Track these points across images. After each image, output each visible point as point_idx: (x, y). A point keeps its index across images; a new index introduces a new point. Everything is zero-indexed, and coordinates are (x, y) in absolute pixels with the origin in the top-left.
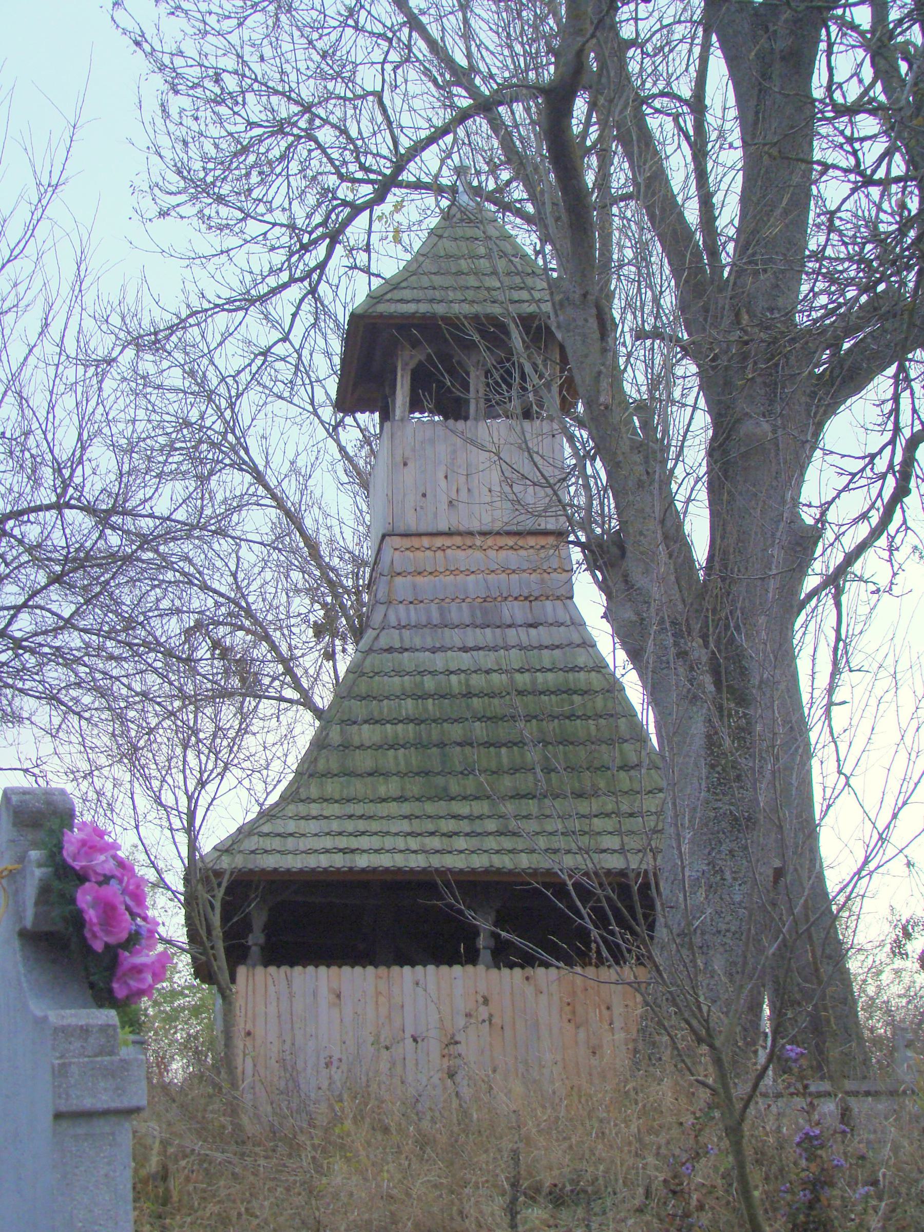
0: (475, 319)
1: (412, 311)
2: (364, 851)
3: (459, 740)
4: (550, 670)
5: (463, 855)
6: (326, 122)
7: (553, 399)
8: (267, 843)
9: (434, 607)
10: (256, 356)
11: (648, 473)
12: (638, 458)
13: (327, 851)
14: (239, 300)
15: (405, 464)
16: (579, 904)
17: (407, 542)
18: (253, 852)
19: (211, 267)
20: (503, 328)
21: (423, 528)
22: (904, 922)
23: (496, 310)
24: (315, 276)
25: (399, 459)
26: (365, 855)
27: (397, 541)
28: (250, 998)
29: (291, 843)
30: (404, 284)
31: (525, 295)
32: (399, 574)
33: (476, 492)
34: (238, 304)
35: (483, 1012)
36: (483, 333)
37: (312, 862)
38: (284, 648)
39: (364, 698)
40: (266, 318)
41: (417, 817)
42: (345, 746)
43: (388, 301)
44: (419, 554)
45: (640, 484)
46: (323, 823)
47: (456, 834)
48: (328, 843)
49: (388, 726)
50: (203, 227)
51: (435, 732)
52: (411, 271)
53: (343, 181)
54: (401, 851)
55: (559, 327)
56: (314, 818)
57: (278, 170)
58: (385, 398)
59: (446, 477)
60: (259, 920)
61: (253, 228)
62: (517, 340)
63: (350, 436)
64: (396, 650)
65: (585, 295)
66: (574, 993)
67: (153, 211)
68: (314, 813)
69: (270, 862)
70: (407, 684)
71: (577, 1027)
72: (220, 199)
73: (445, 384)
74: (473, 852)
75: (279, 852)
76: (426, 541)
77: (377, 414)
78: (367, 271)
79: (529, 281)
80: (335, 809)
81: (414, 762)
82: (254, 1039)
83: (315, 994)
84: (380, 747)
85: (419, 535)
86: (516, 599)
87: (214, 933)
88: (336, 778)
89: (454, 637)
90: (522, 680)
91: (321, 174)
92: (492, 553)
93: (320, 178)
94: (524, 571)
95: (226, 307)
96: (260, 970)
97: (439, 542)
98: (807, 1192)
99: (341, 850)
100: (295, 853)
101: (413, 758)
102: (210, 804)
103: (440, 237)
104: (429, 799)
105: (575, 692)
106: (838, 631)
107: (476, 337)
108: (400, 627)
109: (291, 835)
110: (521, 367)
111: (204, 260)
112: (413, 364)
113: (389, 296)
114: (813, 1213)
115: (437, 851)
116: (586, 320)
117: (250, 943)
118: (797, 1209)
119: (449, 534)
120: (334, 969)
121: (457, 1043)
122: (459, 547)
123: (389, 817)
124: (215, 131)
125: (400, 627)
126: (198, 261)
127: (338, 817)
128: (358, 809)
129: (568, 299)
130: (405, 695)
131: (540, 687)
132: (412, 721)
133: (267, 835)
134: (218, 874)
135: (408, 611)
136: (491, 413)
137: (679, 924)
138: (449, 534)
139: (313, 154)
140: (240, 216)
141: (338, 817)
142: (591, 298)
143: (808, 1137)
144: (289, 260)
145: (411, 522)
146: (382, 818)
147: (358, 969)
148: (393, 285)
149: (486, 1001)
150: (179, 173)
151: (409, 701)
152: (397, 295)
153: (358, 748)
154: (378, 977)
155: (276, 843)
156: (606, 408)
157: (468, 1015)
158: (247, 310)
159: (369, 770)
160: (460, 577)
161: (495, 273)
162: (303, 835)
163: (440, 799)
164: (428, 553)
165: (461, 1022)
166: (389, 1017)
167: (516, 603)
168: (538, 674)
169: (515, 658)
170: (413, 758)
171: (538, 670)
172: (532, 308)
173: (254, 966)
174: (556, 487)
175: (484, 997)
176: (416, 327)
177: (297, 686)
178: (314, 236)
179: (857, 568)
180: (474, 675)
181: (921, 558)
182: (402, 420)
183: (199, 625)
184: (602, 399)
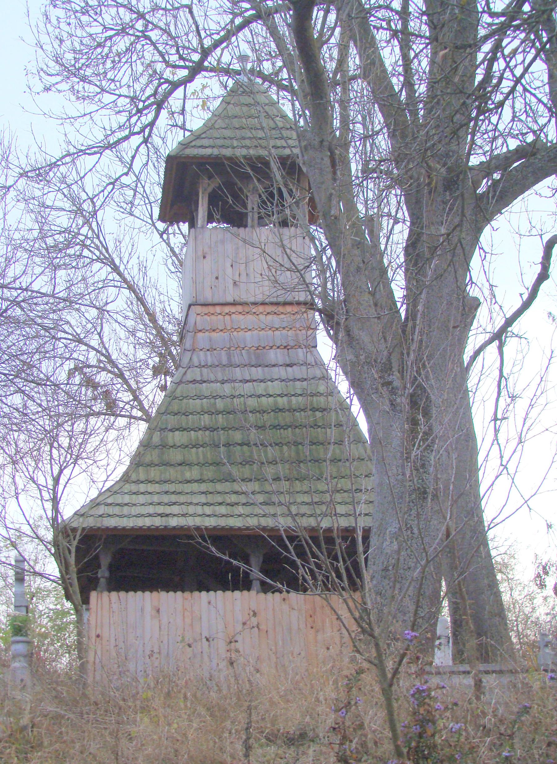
0: (248, 158)
1: (209, 154)
2: (174, 515)
3: (240, 442)
4: (301, 395)
5: (240, 518)
6: (156, 27)
7: (303, 212)
8: (110, 510)
9: (223, 353)
10: (108, 185)
11: (364, 262)
12: (357, 252)
13: (150, 515)
14: (97, 147)
15: (204, 257)
16: (288, 543)
17: (206, 310)
18: (100, 516)
19: (77, 125)
20: (267, 164)
21: (216, 301)
22: (543, 564)
23: (263, 153)
24: (147, 131)
25: (200, 253)
26: (175, 518)
27: (199, 309)
28: (99, 613)
29: (126, 510)
30: (203, 136)
31: (282, 143)
32: (200, 331)
33: (252, 276)
34: (96, 149)
35: (254, 621)
36: (253, 168)
37: (140, 523)
38: (132, 383)
39: (176, 414)
40: (121, 160)
41: (211, 493)
42: (164, 446)
43: (192, 147)
44: (213, 317)
45: (358, 270)
46: (148, 497)
47: (237, 504)
48: (151, 510)
49: (192, 432)
50: (73, 98)
51: (222, 436)
52: (209, 126)
53: (167, 67)
54: (199, 515)
55: (304, 164)
56: (142, 493)
57: (124, 60)
58: (192, 213)
59: (232, 266)
60: (105, 561)
61: (107, 98)
62: (277, 173)
63: (177, 241)
64: (198, 382)
65: (322, 142)
66: (315, 609)
67: (39, 87)
68: (142, 490)
69: (112, 523)
70: (205, 405)
71: (317, 631)
72: (84, 79)
73: (228, 202)
74: (248, 516)
75: (118, 516)
76: (218, 309)
77: (187, 224)
78: (183, 128)
79: (285, 133)
80: (156, 488)
81: (209, 456)
82: (102, 640)
83: (142, 610)
84: (187, 446)
85: (214, 305)
86: (278, 347)
87: (71, 568)
88: (157, 468)
89: (238, 373)
90: (282, 402)
91: (153, 62)
92: (262, 317)
93: (152, 64)
94: (284, 328)
95: (88, 152)
96: (106, 594)
97: (227, 309)
98: (418, 727)
99: (159, 515)
100: (129, 516)
101: (209, 453)
102: (67, 483)
103: (229, 103)
104: (219, 481)
105: (317, 410)
106: (501, 371)
107: (251, 173)
108: (200, 366)
109: (126, 504)
110: (280, 190)
111: (72, 120)
112: (210, 189)
113: (193, 144)
114: (422, 740)
115: (223, 516)
116: (322, 159)
117: (99, 575)
118: (410, 738)
119: (234, 304)
120: (155, 594)
121: (236, 641)
122: (240, 313)
123: (193, 493)
124: (79, 33)
125: (200, 366)
126: (68, 121)
127: (158, 493)
128: (171, 487)
129: (310, 145)
130: (203, 412)
131: (294, 407)
132: (208, 429)
133: (111, 504)
134: (74, 530)
135: (206, 356)
136: (261, 222)
137: (383, 563)
138: (234, 304)
139: (146, 47)
140: (99, 90)
141: (158, 493)
142: (326, 143)
143: (419, 691)
144: (129, 120)
145: (208, 296)
146: (187, 493)
147: (171, 594)
148: (197, 136)
149: (255, 614)
150: (57, 62)
151: (206, 416)
152: (199, 143)
153: (172, 447)
154: (185, 599)
155: (116, 510)
156: (336, 218)
157: (244, 624)
158: (101, 154)
159: (179, 462)
160: (241, 333)
161: (262, 128)
162: (135, 505)
163: (227, 481)
164: (220, 316)
165: (239, 627)
166: (192, 625)
167: (278, 350)
168: (293, 397)
169: (275, 387)
170: (209, 453)
171: (293, 395)
172: (287, 152)
173: (102, 592)
174: (302, 272)
175: (254, 611)
176: (209, 164)
177: (142, 409)
178: (146, 104)
179: (515, 328)
180: (250, 398)
181: (554, 320)
182: (203, 227)
183: (76, 368)
184: (333, 212)
